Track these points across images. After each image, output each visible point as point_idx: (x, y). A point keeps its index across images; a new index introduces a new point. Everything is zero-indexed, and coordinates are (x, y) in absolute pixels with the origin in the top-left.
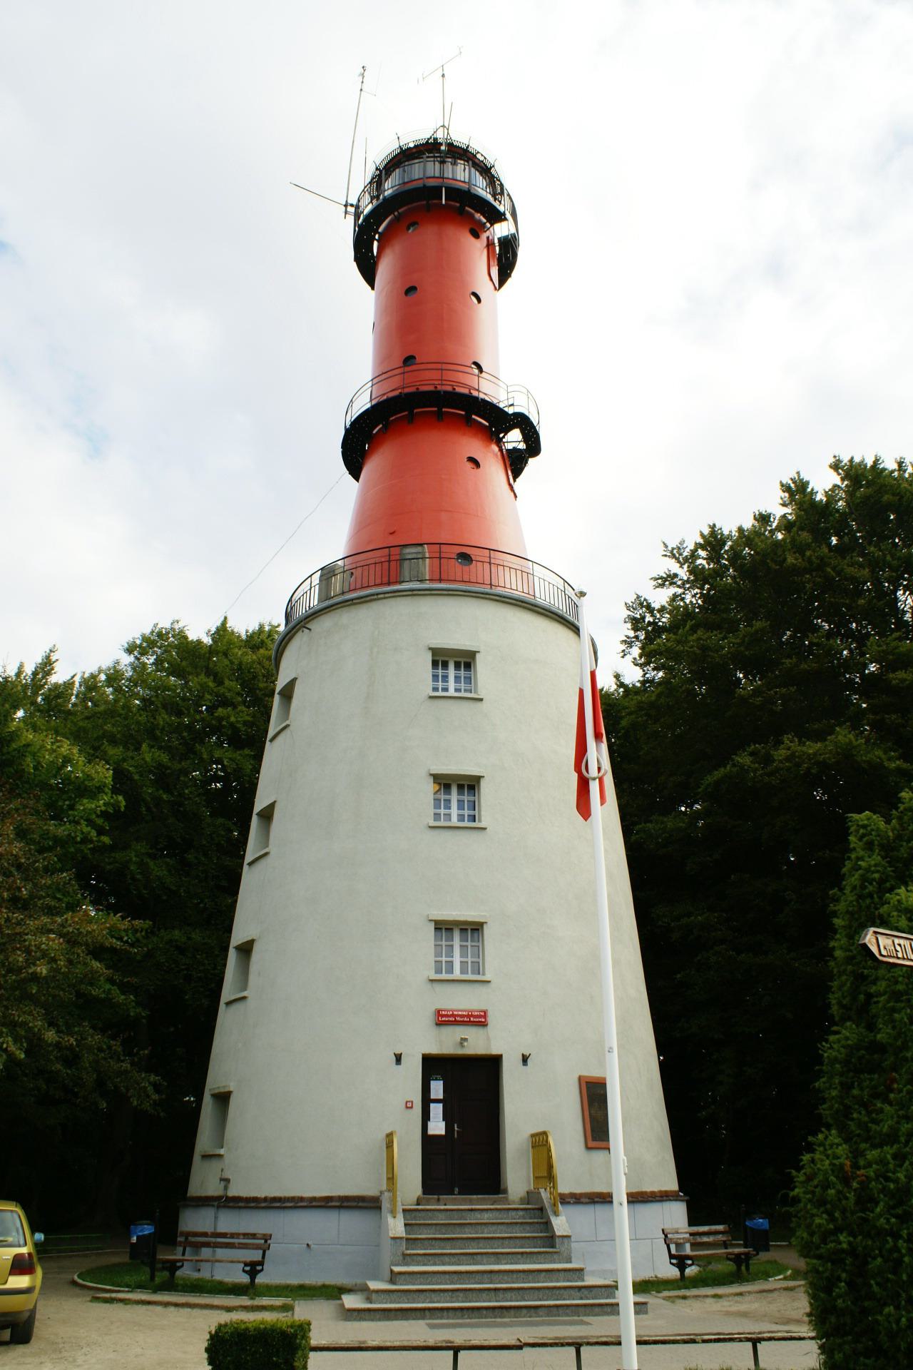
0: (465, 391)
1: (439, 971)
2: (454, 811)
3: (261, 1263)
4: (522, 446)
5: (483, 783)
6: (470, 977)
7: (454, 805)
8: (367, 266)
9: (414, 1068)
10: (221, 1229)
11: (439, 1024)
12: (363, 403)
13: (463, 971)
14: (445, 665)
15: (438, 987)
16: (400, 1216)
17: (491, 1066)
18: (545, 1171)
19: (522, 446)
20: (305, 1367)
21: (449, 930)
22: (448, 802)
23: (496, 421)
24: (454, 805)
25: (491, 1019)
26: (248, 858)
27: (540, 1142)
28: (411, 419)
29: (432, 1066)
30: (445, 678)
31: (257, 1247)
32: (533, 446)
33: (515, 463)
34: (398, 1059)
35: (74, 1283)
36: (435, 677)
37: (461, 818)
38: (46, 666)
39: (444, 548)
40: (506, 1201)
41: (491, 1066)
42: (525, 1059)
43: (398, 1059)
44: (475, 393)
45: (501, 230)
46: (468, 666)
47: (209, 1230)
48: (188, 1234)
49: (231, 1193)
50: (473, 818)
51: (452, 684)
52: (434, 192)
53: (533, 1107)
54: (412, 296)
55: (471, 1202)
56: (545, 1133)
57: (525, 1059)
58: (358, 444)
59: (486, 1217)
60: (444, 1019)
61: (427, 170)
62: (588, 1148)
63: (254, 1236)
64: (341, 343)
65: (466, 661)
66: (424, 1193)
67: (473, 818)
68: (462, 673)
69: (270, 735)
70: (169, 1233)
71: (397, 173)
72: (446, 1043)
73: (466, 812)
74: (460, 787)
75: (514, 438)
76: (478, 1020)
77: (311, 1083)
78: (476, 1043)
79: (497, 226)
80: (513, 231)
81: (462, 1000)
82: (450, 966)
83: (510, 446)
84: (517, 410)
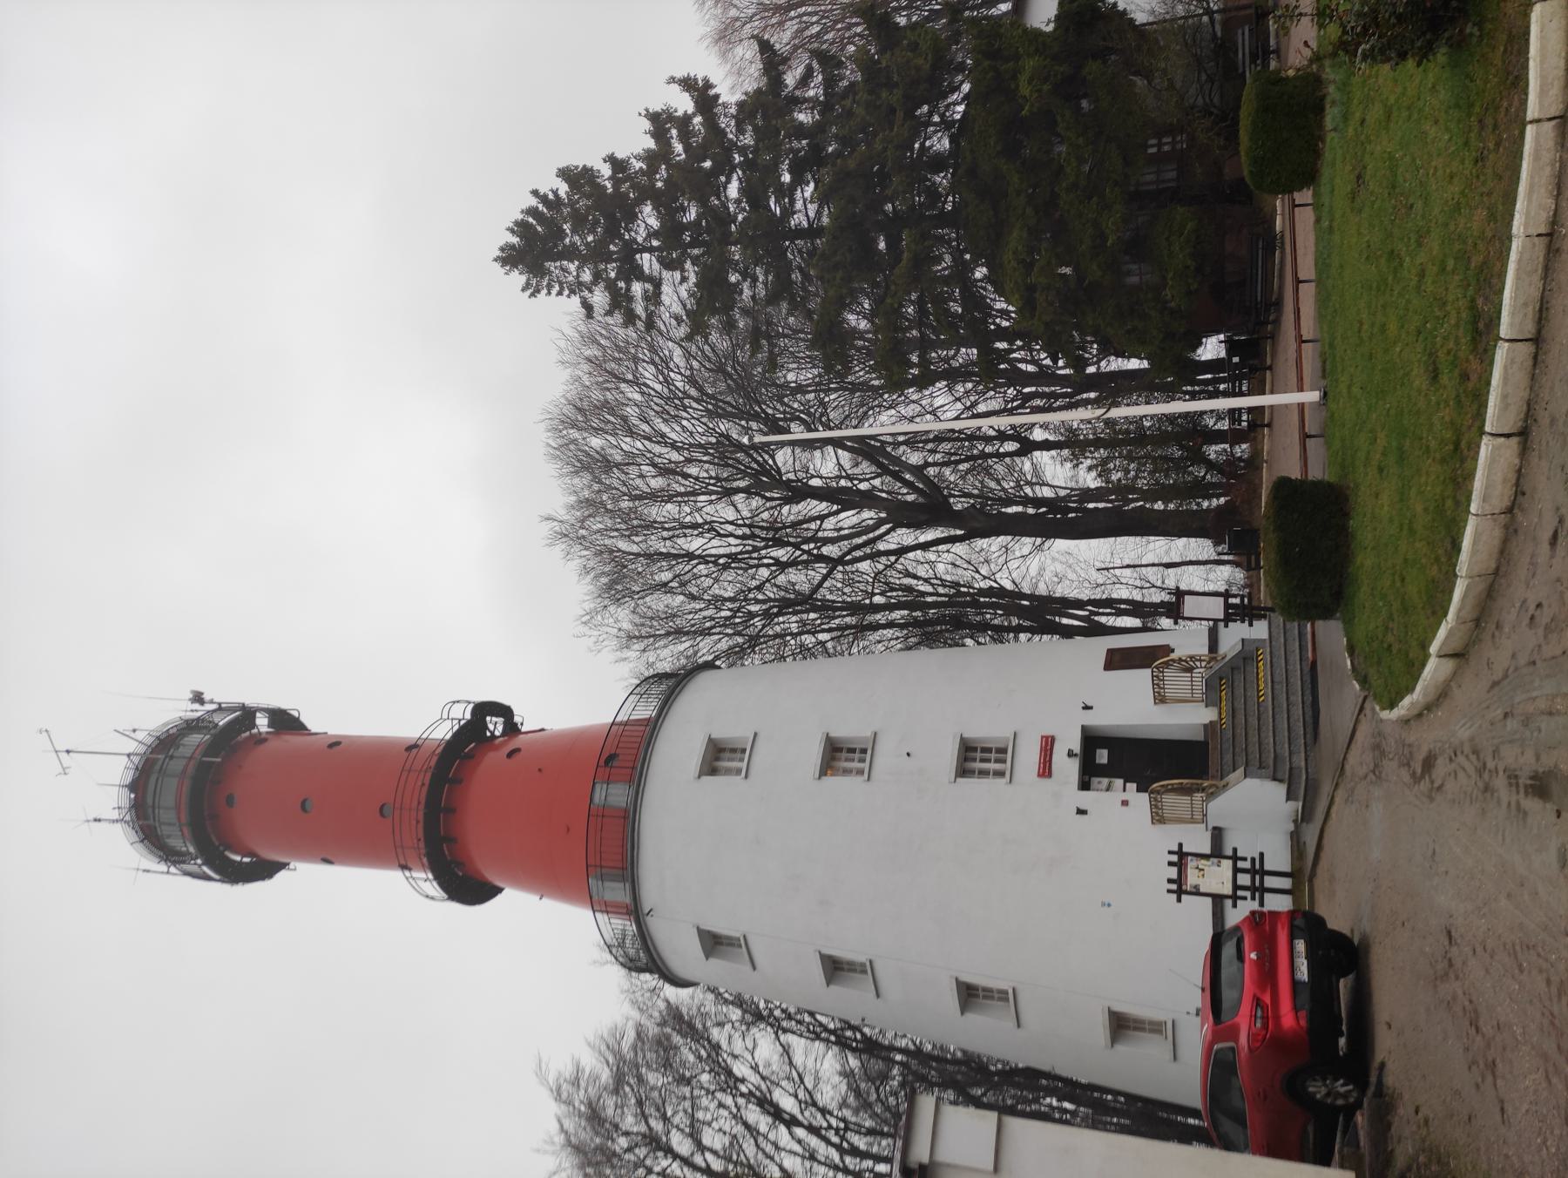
0: (435, 759)
8: (264, 870)
9: (1086, 799)
11: (1050, 775)
17: (1092, 740)
20: (1061, 4)
25: (1048, 733)
28: (451, 811)
32: (505, 711)
33: (512, 728)
34: (1081, 812)
37: (862, 760)
39: (591, 862)
41: (1092, 740)
42: (1087, 708)
43: (1081, 812)
44: (433, 763)
46: (722, 750)
52: (203, 768)
57: (1087, 708)
58: (468, 887)
60: (1046, 770)
61: (170, 793)
67: (864, 751)
71: (164, 830)
72: (1067, 769)
73: (857, 755)
75: (495, 725)
76: (1048, 744)
81: (1028, 756)
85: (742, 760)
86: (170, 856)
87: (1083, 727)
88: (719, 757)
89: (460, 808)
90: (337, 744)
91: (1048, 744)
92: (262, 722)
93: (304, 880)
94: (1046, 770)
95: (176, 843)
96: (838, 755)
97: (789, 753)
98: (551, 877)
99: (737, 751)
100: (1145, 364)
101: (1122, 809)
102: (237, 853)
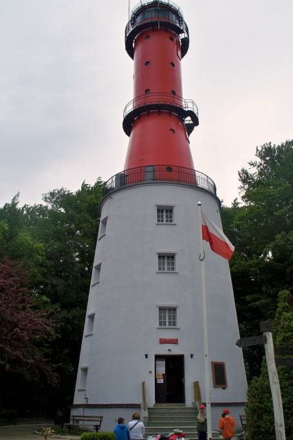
1: (160, 325)
2: (166, 267)
3: (100, 426)
4: (191, 122)
5: (177, 309)
6: (172, 327)
7: (165, 217)
8: (130, 51)
10: (85, 415)
11: (161, 343)
12: (130, 109)
13: (170, 325)
14: (162, 211)
15: (159, 330)
16: (147, 410)
18: (198, 395)
19: (191, 122)
21: (163, 257)
22: (164, 263)
23: (183, 113)
24: (165, 217)
26: (92, 284)
27: (196, 385)
28: (159, 113)
29: (158, 357)
30: (162, 216)
31: (97, 421)
32: (196, 121)
33: (190, 129)
34: (146, 356)
35: (35, 433)
36: (158, 216)
38: (14, 204)
40: (185, 405)
41: (180, 359)
42: (192, 356)
43: (146, 356)
45: (182, 36)
46: (171, 211)
47: (82, 415)
48: (74, 417)
49: (89, 403)
50: (171, 221)
51: (166, 267)
53: (196, 374)
54: (149, 66)
55: (172, 406)
56: (198, 382)
57: (192, 356)
58: (129, 124)
59: (177, 411)
60: (163, 341)
61: (152, 16)
62: (214, 387)
63: (97, 417)
64: (120, 82)
65: (170, 210)
66: (156, 402)
68: (169, 214)
69: (98, 238)
70: (67, 416)
72: (164, 350)
74: (168, 257)
75: (188, 120)
76: (175, 342)
77: (115, 361)
78: (175, 350)
79: (180, 35)
80: (186, 36)
82: (165, 322)
83: (187, 122)
84: (189, 109)
85: (167, 221)
86: (133, 20)
87: (183, 355)
88: (165, 213)
89: (159, 115)
90: (174, 66)
91: (175, 342)
92: (182, 36)
93: (127, 67)
94: (163, 341)
95: (139, 20)
96: (167, 259)
97: (165, 239)
98: (136, 154)
99: (170, 219)
100: (269, 336)
101: (149, 375)
102: (138, 37)
